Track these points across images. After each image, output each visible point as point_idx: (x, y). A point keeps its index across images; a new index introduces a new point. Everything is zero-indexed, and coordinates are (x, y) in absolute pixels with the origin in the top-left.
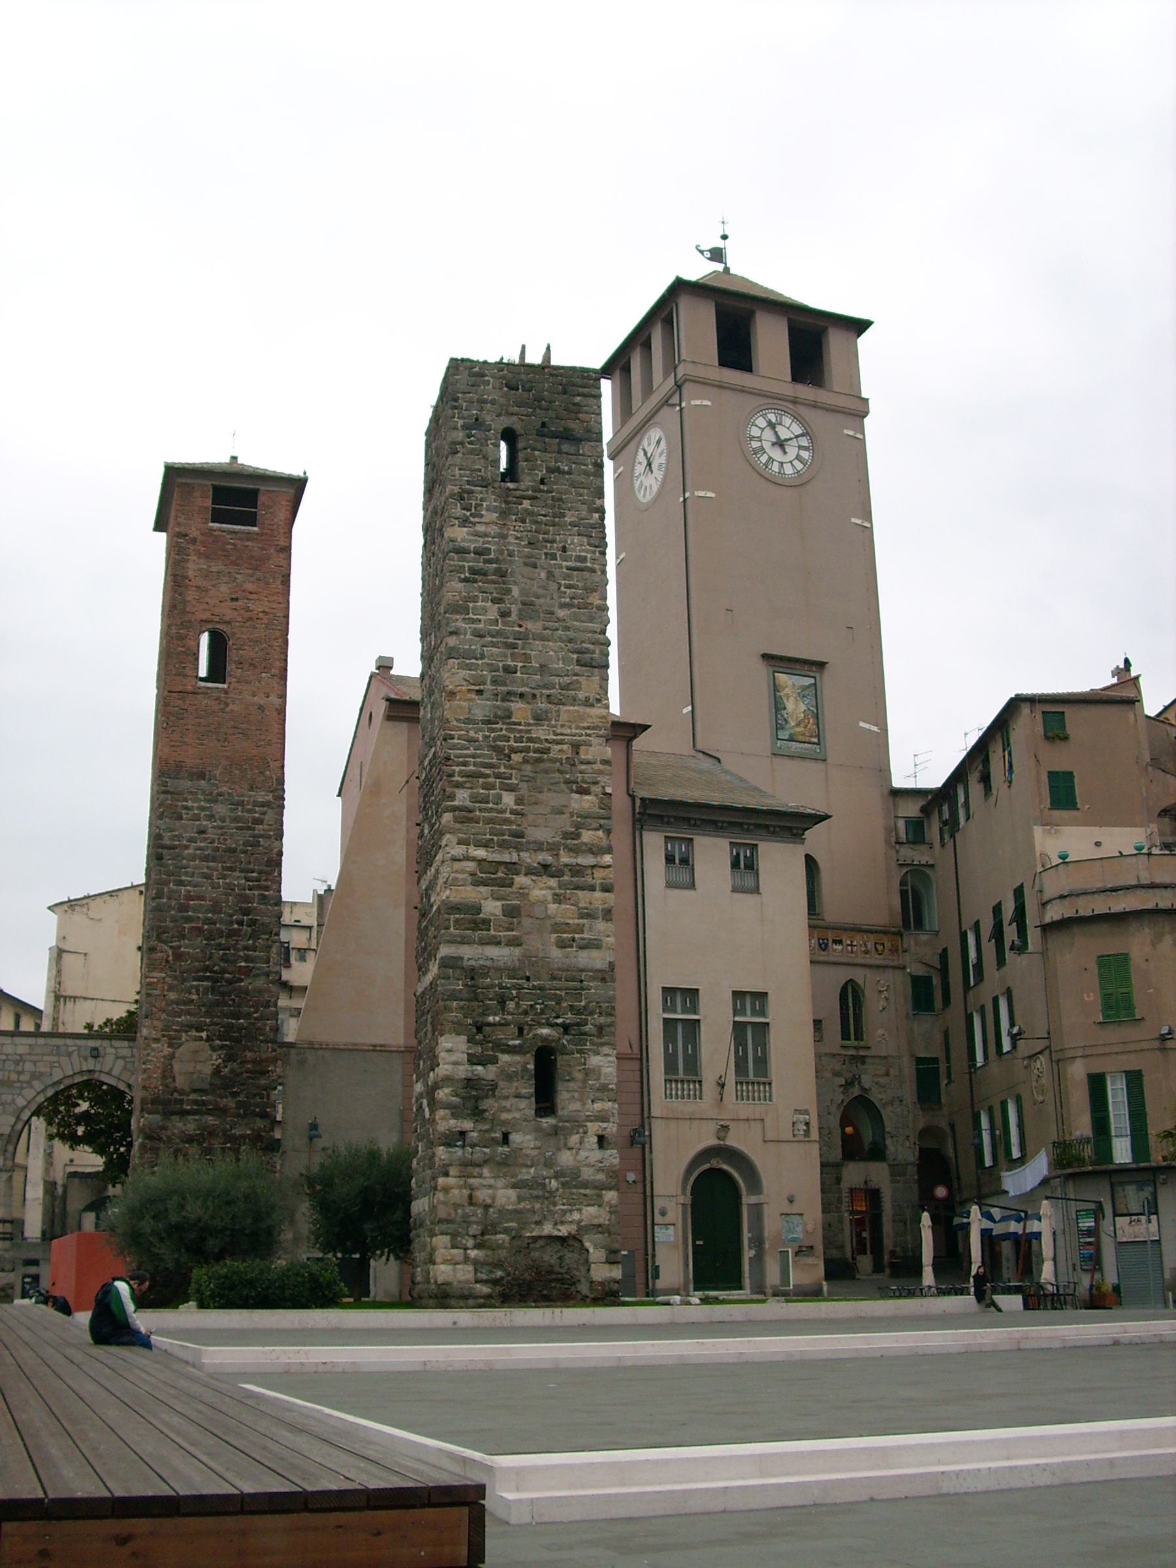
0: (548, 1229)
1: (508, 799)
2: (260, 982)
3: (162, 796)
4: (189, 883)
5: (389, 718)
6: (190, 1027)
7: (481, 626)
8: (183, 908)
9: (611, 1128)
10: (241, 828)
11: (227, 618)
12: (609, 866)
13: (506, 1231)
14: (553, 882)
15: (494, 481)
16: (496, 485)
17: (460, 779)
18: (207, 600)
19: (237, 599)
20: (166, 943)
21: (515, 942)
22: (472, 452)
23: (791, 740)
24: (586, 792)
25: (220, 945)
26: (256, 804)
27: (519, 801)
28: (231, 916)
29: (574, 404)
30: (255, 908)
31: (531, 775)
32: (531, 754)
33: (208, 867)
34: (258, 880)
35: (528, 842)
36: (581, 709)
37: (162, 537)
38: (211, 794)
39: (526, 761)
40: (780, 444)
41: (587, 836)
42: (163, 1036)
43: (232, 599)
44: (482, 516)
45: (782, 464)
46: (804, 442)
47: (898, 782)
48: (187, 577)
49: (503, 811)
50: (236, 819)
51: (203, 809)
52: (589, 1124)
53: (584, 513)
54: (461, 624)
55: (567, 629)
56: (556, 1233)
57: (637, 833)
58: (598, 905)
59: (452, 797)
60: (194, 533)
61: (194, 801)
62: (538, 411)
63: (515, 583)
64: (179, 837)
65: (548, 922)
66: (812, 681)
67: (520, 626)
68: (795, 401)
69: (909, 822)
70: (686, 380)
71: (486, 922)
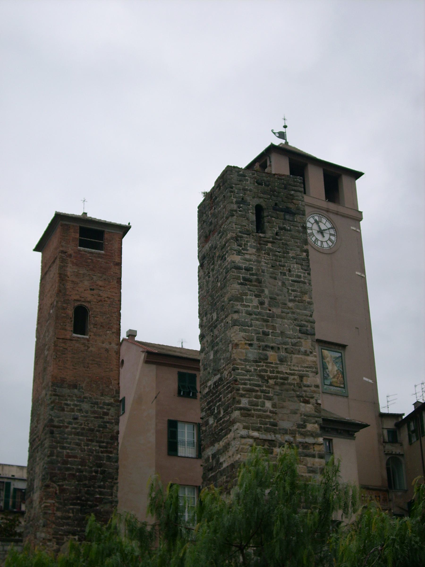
1: (268, 405)
3: (53, 397)
5: (147, 362)
7: (250, 309)
8: (65, 462)
11: (89, 300)
12: (322, 444)
15: (253, 232)
16: (254, 234)
18: (77, 288)
19: (93, 290)
20: (54, 482)
22: (241, 216)
23: (331, 385)
24: (307, 402)
25: (85, 484)
26: (105, 404)
27: (274, 406)
28: (91, 467)
29: (291, 195)
30: (104, 463)
31: (280, 392)
32: (279, 380)
33: (79, 439)
34: (106, 447)
35: (280, 429)
36: (303, 357)
37: (39, 255)
38: (80, 397)
39: (276, 384)
40: (321, 232)
42: (54, 538)
43: (91, 289)
44: (247, 250)
45: (322, 242)
46: (332, 231)
47: (383, 410)
48: (66, 275)
49: (265, 411)
50: (94, 412)
51: (76, 405)
53: (299, 253)
54: (239, 307)
55: (293, 313)
58: (317, 465)
59: (239, 402)
60: (70, 251)
61: (73, 400)
62: (273, 197)
63: (266, 287)
64: (63, 421)
66: (340, 355)
67: (270, 310)
68: (328, 211)
69: (390, 431)
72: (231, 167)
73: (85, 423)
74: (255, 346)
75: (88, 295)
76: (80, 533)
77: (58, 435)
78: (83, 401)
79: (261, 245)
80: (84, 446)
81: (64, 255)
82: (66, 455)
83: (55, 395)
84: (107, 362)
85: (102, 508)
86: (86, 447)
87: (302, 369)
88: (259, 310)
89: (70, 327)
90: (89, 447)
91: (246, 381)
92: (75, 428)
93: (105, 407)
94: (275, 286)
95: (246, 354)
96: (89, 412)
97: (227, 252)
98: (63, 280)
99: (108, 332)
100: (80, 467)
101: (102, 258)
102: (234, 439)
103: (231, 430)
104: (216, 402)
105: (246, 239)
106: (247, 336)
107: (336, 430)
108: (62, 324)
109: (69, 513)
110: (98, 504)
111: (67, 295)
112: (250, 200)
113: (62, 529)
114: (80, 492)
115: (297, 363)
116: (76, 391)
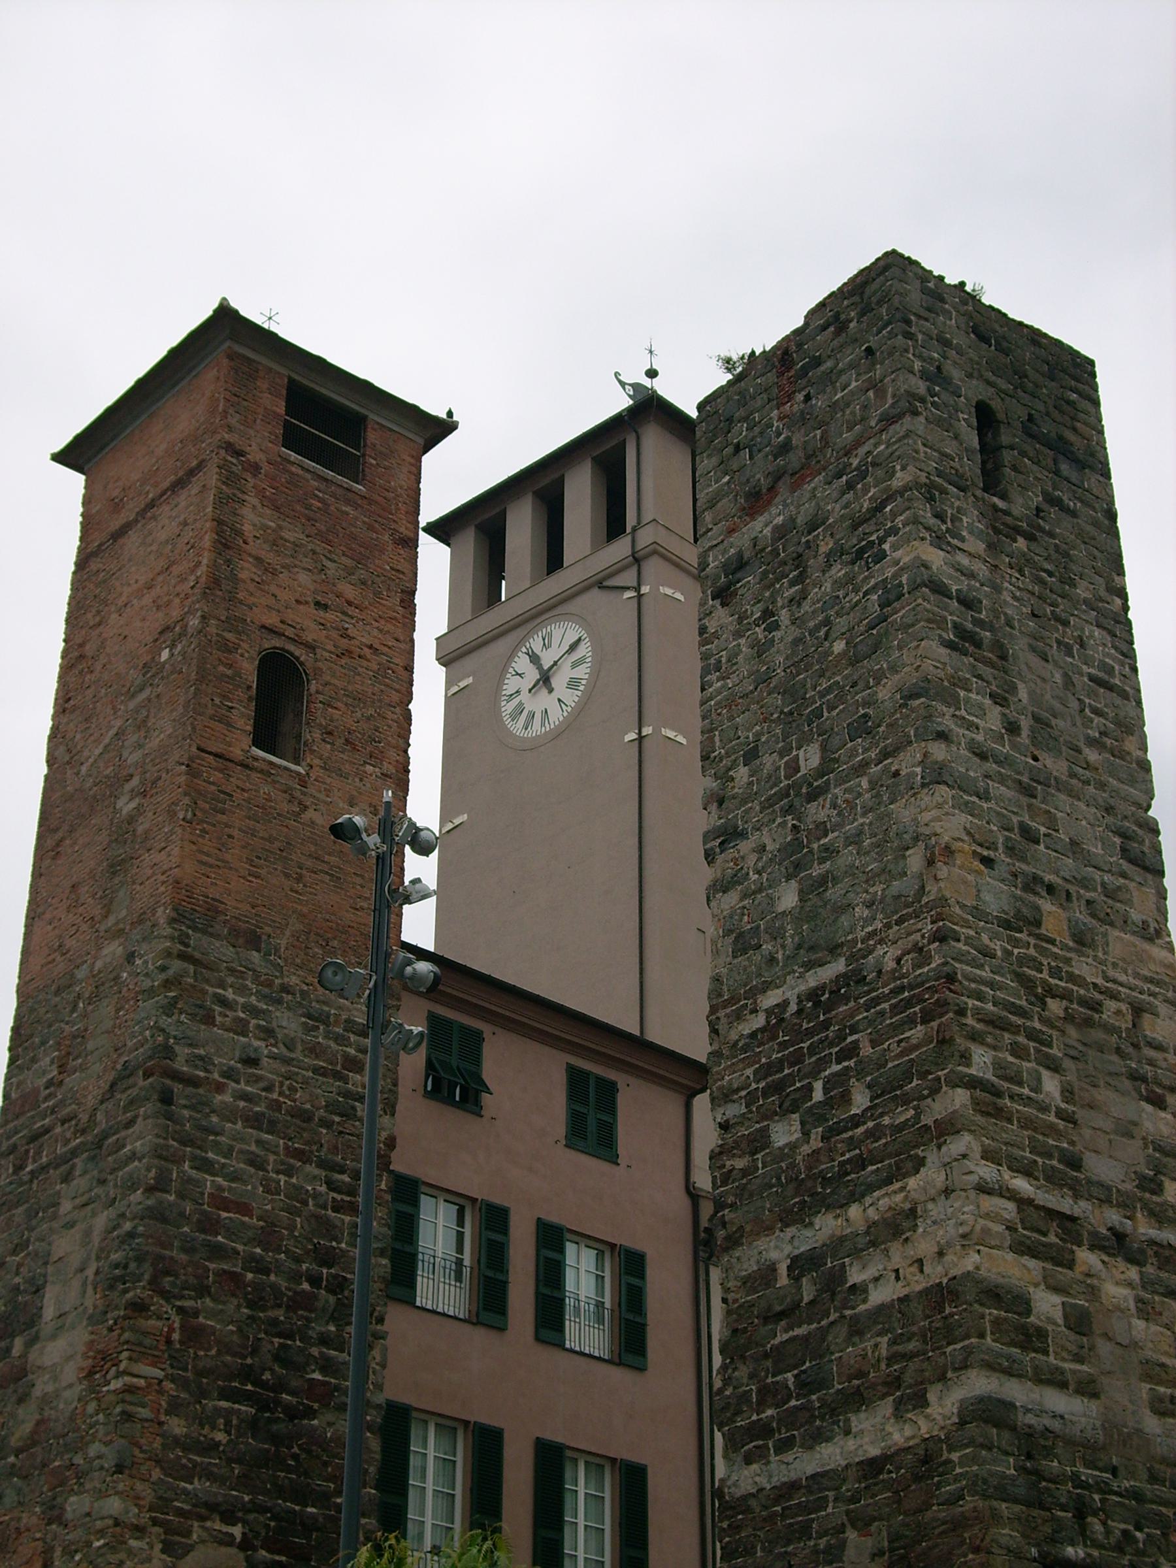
1: (1051, 1085)
3: (177, 965)
4: (221, 1171)
6: (213, 1508)
7: (980, 738)
11: (309, 637)
18: (273, 589)
19: (325, 607)
20: (166, 1295)
21: (1088, 1389)
25: (274, 1322)
27: (1068, 1093)
33: (259, 1142)
38: (270, 984)
39: (1069, 1018)
42: (155, 1522)
48: (239, 533)
49: (1044, 1109)
50: (314, 1050)
51: (255, 1012)
55: (1102, 786)
57: (702, 1266)
59: (965, 1058)
60: (255, 454)
61: (242, 990)
64: (205, 1062)
67: (1036, 759)
70: (655, 552)
72: (902, 256)
73: (281, 1084)
74: (1002, 870)
75: (307, 621)
76: (251, 1517)
78: (279, 1001)
79: (1001, 530)
80: (278, 1172)
81: (234, 461)
82: (211, 1195)
83: (183, 956)
84: (362, 876)
85: (330, 1424)
86: (282, 1178)
89: (243, 718)
90: (294, 1180)
91: (983, 988)
92: (245, 1097)
93: (353, 1038)
94: (1044, 680)
95: (979, 891)
96: (299, 1047)
97: (894, 531)
99: (369, 768)
100: (258, 1250)
101: (356, 506)
102: (947, 1192)
103: (921, 1162)
104: (824, 1062)
105: (957, 503)
106: (979, 828)
108: (217, 701)
109: (213, 1427)
110: (316, 1406)
111: (241, 602)
112: (960, 380)
113: (186, 1492)
114: (255, 1351)
116: (255, 956)
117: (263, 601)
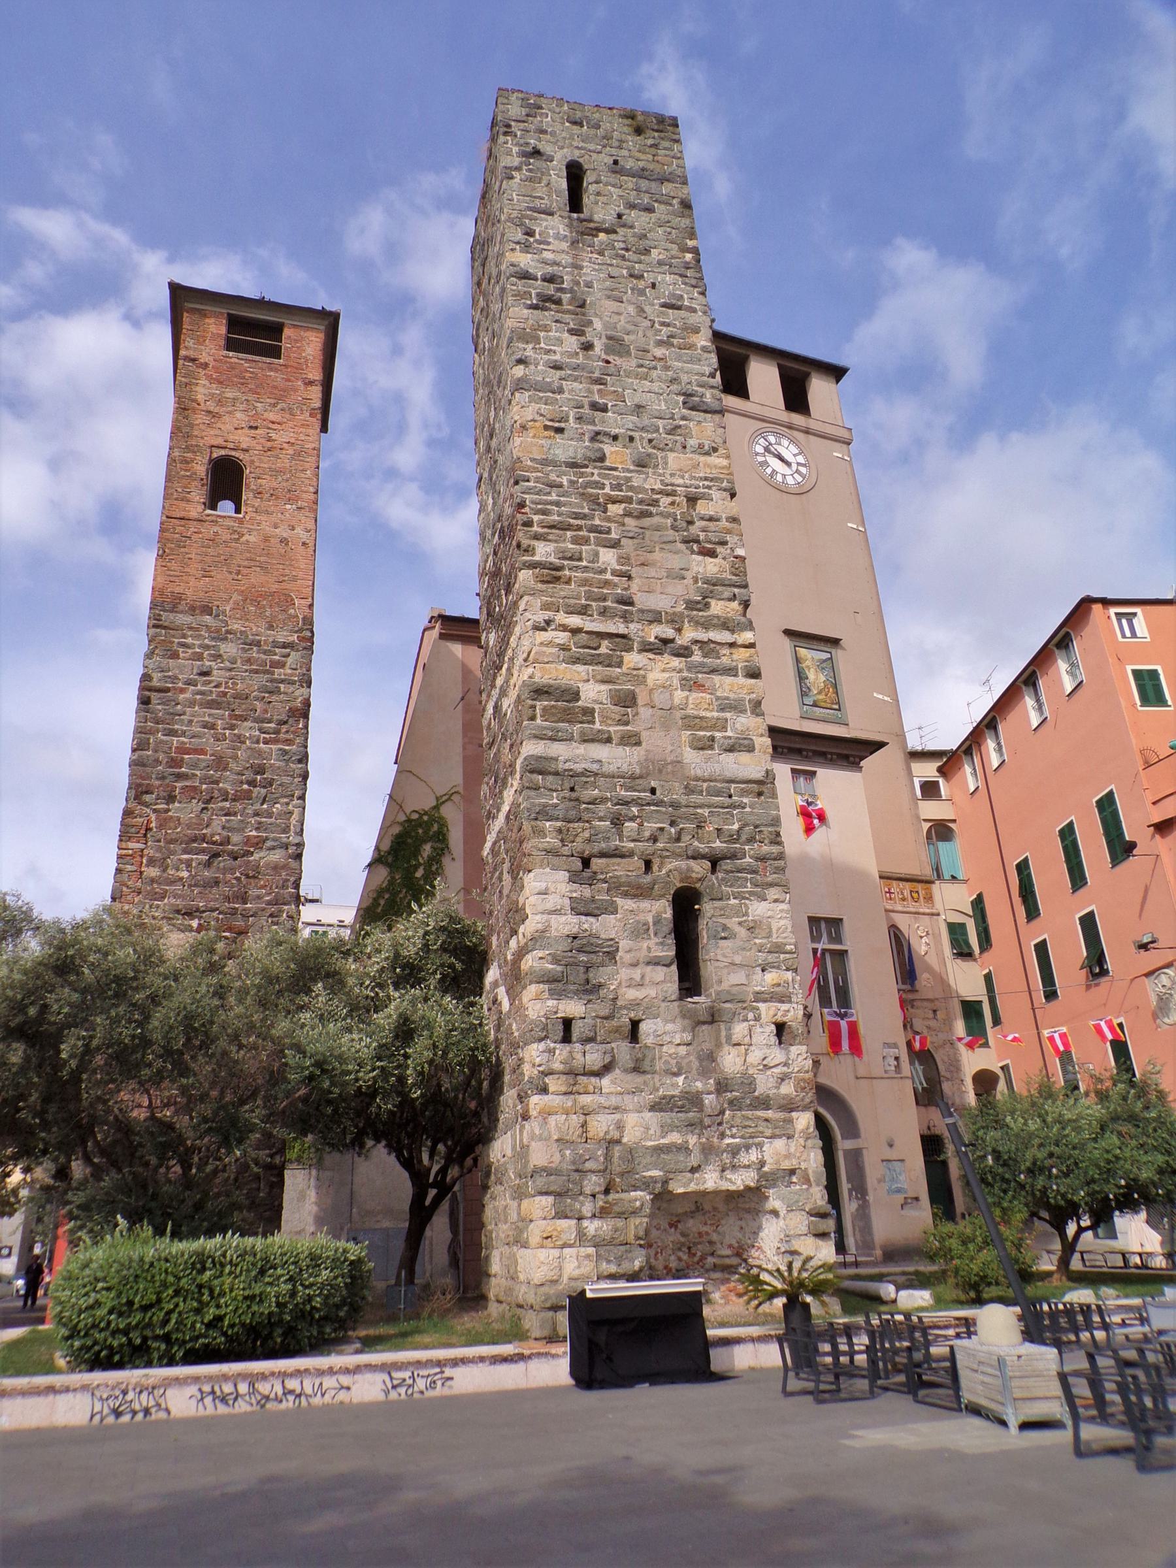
0: (710, 1180)
1: (608, 557)
2: (277, 856)
4: (184, 734)
7: (557, 357)
8: (175, 763)
9: (792, 1013)
10: (256, 671)
11: (244, 446)
13: (646, 1184)
14: (676, 662)
17: (540, 530)
19: (256, 428)
21: (631, 740)
23: (815, 705)
24: (712, 554)
26: (275, 644)
27: (624, 559)
30: (272, 765)
32: (634, 506)
34: (277, 732)
35: (642, 611)
38: (218, 631)
39: (628, 514)
41: (717, 608)
43: (251, 427)
44: (549, 243)
45: (784, 476)
48: (195, 401)
49: (603, 571)
50: (249, 661)
51: (207, 647)
52: (761, 1005)
54: (529, 353)
56: (725, 1186)
61: (199, 637)
64: (174, 679)
65: (678, 714)
66: (829, 656)
71: (588, 712)
73: (227, 683)
75: (244, 439)
77: (160, 707)
78: (226, 639)
86: (227, 732)
87: (693, 482)
88: (580, 359)
91: (549, 507)
98: (185, 409)
99: (288, 507)
101: (276, 371)
107: (823, 754)
115: (680, 470)
117: (212, 433)
